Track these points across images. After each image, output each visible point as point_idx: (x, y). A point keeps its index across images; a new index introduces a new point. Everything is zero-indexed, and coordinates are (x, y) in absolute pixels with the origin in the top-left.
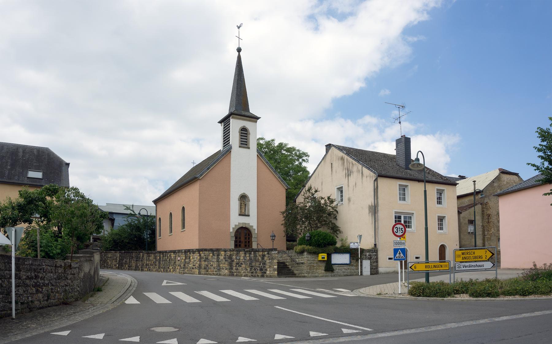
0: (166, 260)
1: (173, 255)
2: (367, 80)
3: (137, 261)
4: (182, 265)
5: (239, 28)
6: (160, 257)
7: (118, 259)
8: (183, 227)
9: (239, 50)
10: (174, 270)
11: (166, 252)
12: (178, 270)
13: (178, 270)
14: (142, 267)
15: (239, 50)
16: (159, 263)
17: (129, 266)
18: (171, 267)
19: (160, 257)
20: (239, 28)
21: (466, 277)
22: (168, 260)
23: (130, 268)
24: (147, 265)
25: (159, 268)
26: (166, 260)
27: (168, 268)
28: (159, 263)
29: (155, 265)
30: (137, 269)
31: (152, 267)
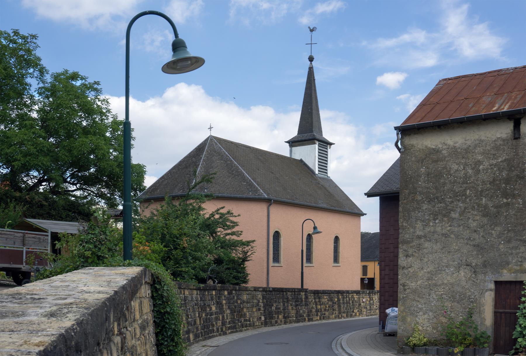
0: (348, 303)
1: (356, 296)
2: (138, 100)
3: (296, 306)
4: (368, 307)
5: (312, 31)
6: (338, 298)
7: (262, 305)
8: (336, 259)
9: (311, 59)
10: (361, 313)
11: (348, 292)
12: (365, 313)
13: (365, 313)
14: (308, 316)
15: (311, 59)
16: (339, 306)
17: (285, 317)
18: (356, 311)
19: (338, 298)
20: (312, 31)
21: (63, 293)
22: (351, 302)
23: (287, 319)
24: (317, 311)
25: (340, 313)
26: (348, 303)
27: (353, 312)
28: (339, 306)
29: (334, 310)
30: (299, 318)
31: (327, 313)
